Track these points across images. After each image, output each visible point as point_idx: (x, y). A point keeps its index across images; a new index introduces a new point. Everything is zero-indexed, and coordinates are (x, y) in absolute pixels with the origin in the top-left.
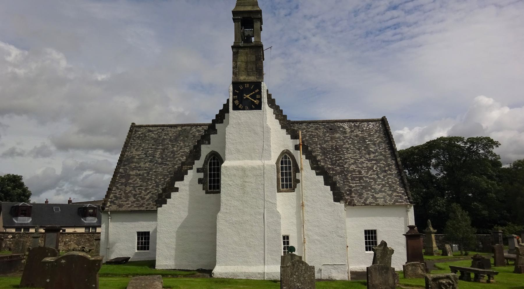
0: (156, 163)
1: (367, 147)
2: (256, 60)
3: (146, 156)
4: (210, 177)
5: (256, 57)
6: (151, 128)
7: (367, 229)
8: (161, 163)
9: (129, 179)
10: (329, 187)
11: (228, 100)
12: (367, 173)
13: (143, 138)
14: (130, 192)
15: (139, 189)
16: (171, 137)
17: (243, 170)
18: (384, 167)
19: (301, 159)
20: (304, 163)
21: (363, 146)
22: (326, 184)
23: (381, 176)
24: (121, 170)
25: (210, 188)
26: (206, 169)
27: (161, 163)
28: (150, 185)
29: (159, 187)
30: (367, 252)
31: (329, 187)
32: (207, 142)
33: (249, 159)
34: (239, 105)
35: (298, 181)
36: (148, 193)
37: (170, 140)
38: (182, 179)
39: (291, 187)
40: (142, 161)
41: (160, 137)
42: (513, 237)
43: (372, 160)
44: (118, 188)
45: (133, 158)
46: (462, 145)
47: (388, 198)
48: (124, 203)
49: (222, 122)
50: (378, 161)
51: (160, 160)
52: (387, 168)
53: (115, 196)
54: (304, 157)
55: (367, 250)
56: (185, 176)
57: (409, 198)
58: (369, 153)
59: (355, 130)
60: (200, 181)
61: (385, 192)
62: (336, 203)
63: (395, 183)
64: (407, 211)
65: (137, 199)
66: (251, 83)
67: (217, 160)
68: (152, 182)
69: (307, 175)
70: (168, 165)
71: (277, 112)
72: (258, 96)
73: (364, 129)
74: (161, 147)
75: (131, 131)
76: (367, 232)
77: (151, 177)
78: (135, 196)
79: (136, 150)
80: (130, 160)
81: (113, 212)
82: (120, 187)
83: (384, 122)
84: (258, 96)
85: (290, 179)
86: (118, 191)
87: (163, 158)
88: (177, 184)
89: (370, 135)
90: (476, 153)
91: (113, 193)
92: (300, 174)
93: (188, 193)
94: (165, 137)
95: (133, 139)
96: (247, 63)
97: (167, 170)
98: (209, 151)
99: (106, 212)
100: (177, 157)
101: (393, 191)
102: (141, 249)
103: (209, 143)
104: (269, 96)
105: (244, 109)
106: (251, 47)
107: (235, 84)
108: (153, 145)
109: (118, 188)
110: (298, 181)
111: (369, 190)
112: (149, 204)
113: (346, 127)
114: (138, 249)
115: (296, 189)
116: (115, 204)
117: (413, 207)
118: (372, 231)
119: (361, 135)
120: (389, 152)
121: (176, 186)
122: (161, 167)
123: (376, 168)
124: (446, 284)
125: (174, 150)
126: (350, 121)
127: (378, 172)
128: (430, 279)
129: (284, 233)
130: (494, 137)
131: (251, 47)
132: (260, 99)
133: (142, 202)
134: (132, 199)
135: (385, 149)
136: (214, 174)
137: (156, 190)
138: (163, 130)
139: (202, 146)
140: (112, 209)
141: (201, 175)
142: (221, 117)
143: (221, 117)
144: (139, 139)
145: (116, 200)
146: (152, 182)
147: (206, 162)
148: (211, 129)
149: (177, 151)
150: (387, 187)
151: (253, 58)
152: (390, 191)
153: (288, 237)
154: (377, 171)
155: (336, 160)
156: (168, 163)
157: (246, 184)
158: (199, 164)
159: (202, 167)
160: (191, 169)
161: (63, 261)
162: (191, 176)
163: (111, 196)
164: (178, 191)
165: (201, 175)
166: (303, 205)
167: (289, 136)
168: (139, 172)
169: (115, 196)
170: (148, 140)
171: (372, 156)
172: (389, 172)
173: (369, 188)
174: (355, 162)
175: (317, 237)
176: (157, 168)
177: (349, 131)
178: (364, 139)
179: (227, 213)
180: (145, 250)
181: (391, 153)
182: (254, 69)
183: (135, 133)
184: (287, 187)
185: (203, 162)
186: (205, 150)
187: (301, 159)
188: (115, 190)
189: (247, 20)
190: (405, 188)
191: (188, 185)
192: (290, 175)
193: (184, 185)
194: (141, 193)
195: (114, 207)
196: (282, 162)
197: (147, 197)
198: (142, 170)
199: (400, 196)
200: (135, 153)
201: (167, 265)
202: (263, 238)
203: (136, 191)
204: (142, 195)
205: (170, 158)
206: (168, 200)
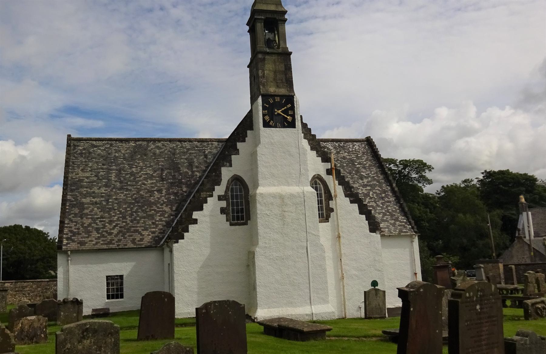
0: (114, 188)
1: (358, 171)
2: (286, 69)
3: (98, 179)
4: (233, 206)
5: (285, 66)
6: (94, 143)
8: (121, 188)
9: (84, 209)
10: (364, 216)
13: (88, 155)
14: (90, 225)
15: (101, 221)
16: (124, 154)
17: (281, 197)
18: (381, 194)
19: (334, 185)
20: (337, 190)
21: (353, 170)
22: (361, 213)
23: (379, 203)
24: (69, 197)
25: (233, 220)
26: (229, 196)
27: (121, 188)
28: (114, 216)
29: (126, 219)
31: (364, 216)
32: (228, 164)
33: (284, 185)
34: (269, 121)
35: (332, 210)
36: (115, 226)
37: (124, 159)
38: (201, 209)
40: (95, 185)
41: (109, 154)
42: (480, 267)
43: (366, 185)
44: (71, 221)
45: (81, 181)
46: (393, 168)
47: (393, 228)
48: (86, 240)
50: (373, 187)
51: (118, 185)
52: (383, 195)
53: (71, 231)
57: (413, 228)
58: (362, 178)
59: (340, 151)
61: (388, 221)
62: (372, 234)
63: (395, 211)
64: (412, 242)
65: (101, 234)
66: (282, 96)
68: (115, 213)
69: (341, 202)
70: (130, 190)
71: (306, 131)
72: (290, 112)
73: (351, 150)
74: (114, 167)
75: (68, 145)
77: (113, 205)
78: (97, 230)
79: (82, 170)
80: (78, 184)
81: (75, 252)
82: (74, 219)
84: (290, 112)
86: (72, 225)
87: (121, 182)
88: (196, 215)
89: (358, 157)
90: (407, 177)
91: (67, 227)
92: (334, 202)
93: (209, 225)
94: (117, 155)
95: (74, 157)
96: (275, 72)
97: (131, 197)
98: (231, 175)
99: (65, 252)
100: (140, 181)
101: (394, 220)
102: (113, 298)
103: (231, 166)
105: (275, 127)
106: (279, 54)
108: (103, 165)
109: (71, 221)
110: (332, 210)
112: (119, 240)
113: (331, 148)
114: (108, 298)
115: (330, 219)
116: (73, 241)
117: (417, 238)
119: (348, 157)
120: (381, 177)
121: (194, 217)
122: (122, 193)
123: (373, 195)
124: (541, 308)
125: (133, 172)
126: (333, 141)
127: (375, 199)
128: (530, 304)
130: (427, 159)
131: (279, 54)
133: (109, 238)
134: (95, 234)
135: (377, 173)
137: (123, 222)
138: (111, 145)
139: (222, 168)
140: (72, 248)
141: (224, 204)
144: (82, 156)
145: (74, 235)
146: (115, 213)
147: (227, 188)
148: (229, 147)
149: (138, 173)
150: (388, 215)
151: (282, 67)
152: (392, 220)
156: (129, 188)
157: (286, 214)
158: (220, 190)
159: (223, 194)
160: (211, 196)
161: (422, 290)
163: (66, 231)
164: (197, 223)
165: (224, 204)
166: (339, 237)
167: (320, 158)
168: (94, 200)
169: (71, 231)
170: (95, 158)
171: (365, 181)
172: (386, 199)
175: (354, 272)
176: (116, 194)
177: (335, 152)
178: (352, 161)
179: (266, 247)
180: (117, 298)
181: (384, 178)
182: (284, 80)
183: (74, 149)
185: (224, 189)
186: (226, 174)
187: (334, 185)
188: (68, 224)
190: (407, 217)
191: (210, 215)
193: (204, 216)
194: (104, 226)
195: (74, 246)
197: (115, 231)
198: (98, 197)
199: (404, 226)
200: (81, 174)
201: (189, 313)
202: (307, 274)
203: (97, 224)
204: (107, 229)
205: (130, 181)
206: (186, 234)
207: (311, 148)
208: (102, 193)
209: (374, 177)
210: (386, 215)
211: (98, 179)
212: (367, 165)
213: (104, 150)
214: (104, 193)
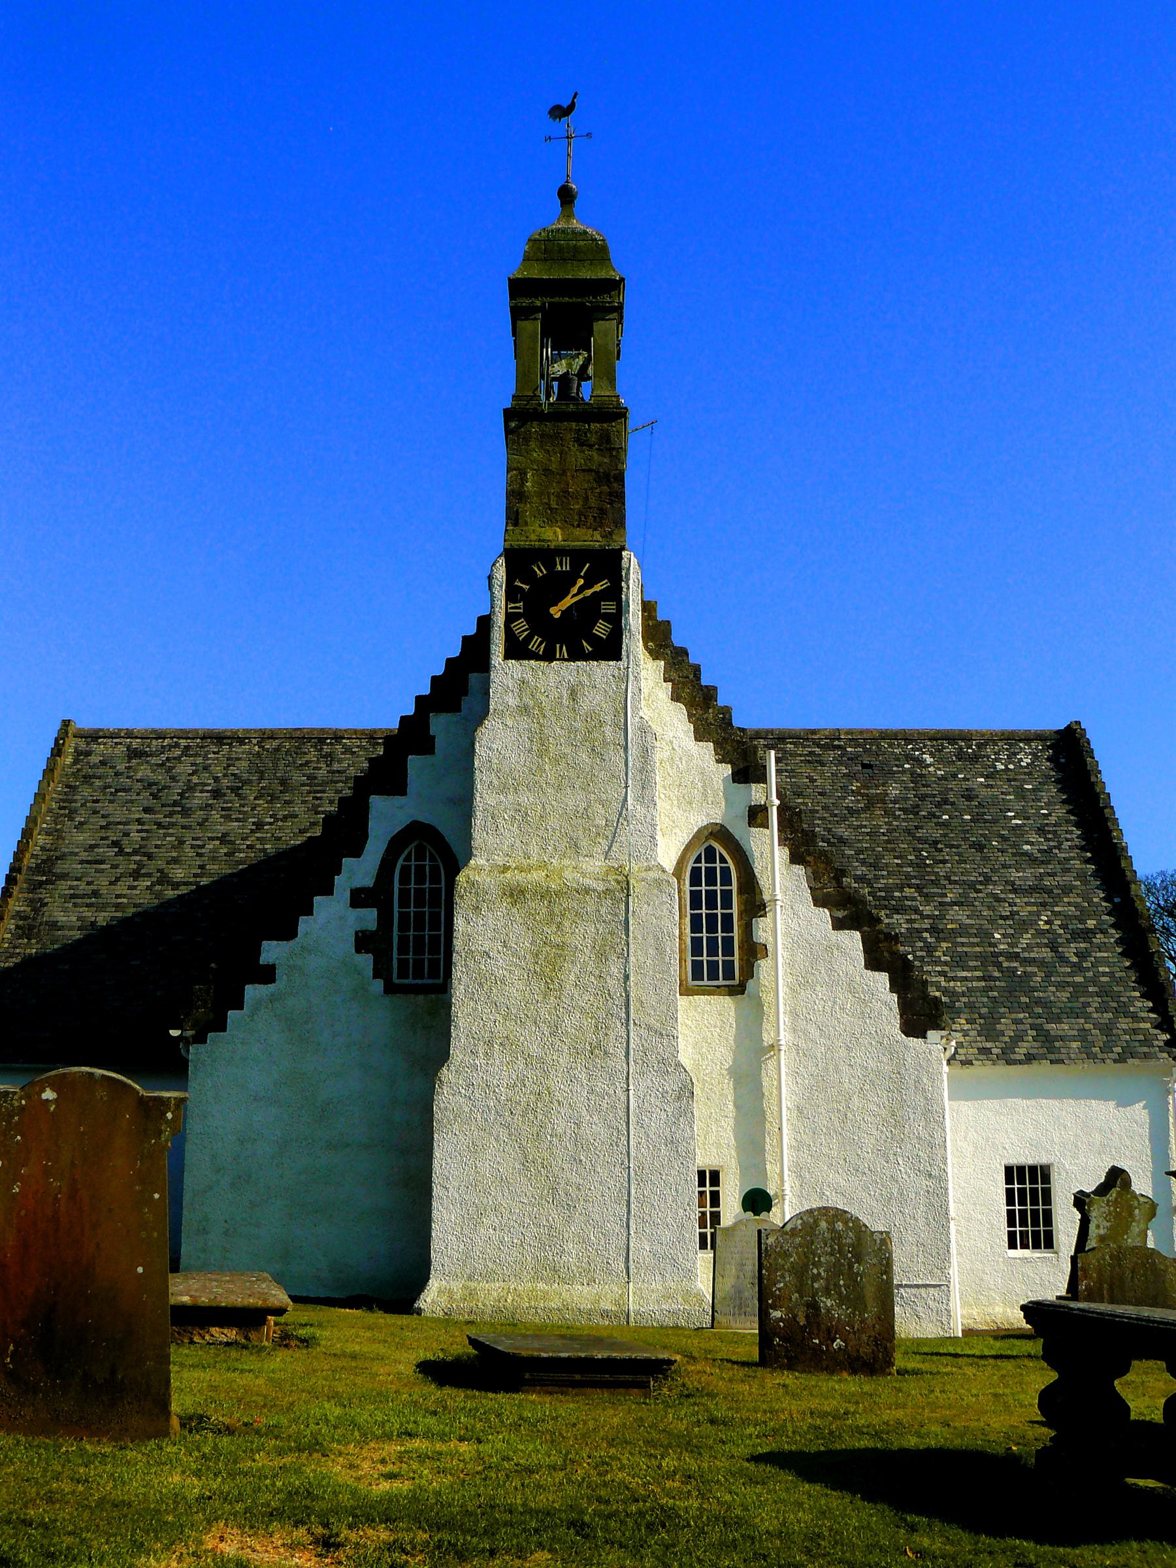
7: (1014, 1161)
11: (485, 623)
12: (1013, 939)
22: (873, 962)
25: (403, 974)
30: (1013, 1253)
34: (529, 639)
39: (729, 974)
49: (456, 708)
52: (1091, 923)
54: (781, 855)
55: (1012, 1245)
56: (302, 918)
60: (363, 942)
61: (1087, 1017)
66: (578, 556)
67: (432, 859)
76: (1012, 1173)
83: (1069, 752)
85: (728, 943)
88: (271, 951)
94: (195, 779)
104: (648, 608)
105: (549, 656)
107: (518, 560)
111: (1026, 1008)
113: (929, 759)
118: (1033, 1169)
129: (705, 1160)
132: (616, 621)
136: (419, 916)
141: (369, 918)
142: (459, 687)
143: (459, 687)
148: (412, 735)
150: (1091, 995)
153: (715, 1177)
154: (1054, 932)
155: (888, 889)
158: (359, 871)
160: (328, 890)
162: (332, 922)
165: (369, 918)
173: (1024, 999)
174: (964, 895)
184: (713, 976)
186: (386, 816)
189: (566, 302)
192: (728, 927)
196: (695, 873)
198: (102, 907)
207: (696, 732)
208: (118, 896)
209: (1067, 860)
210: (1086, 993)
211: (121, 852)
212: (1053, 819)
213: (163, 765)
214: (124, 896)
